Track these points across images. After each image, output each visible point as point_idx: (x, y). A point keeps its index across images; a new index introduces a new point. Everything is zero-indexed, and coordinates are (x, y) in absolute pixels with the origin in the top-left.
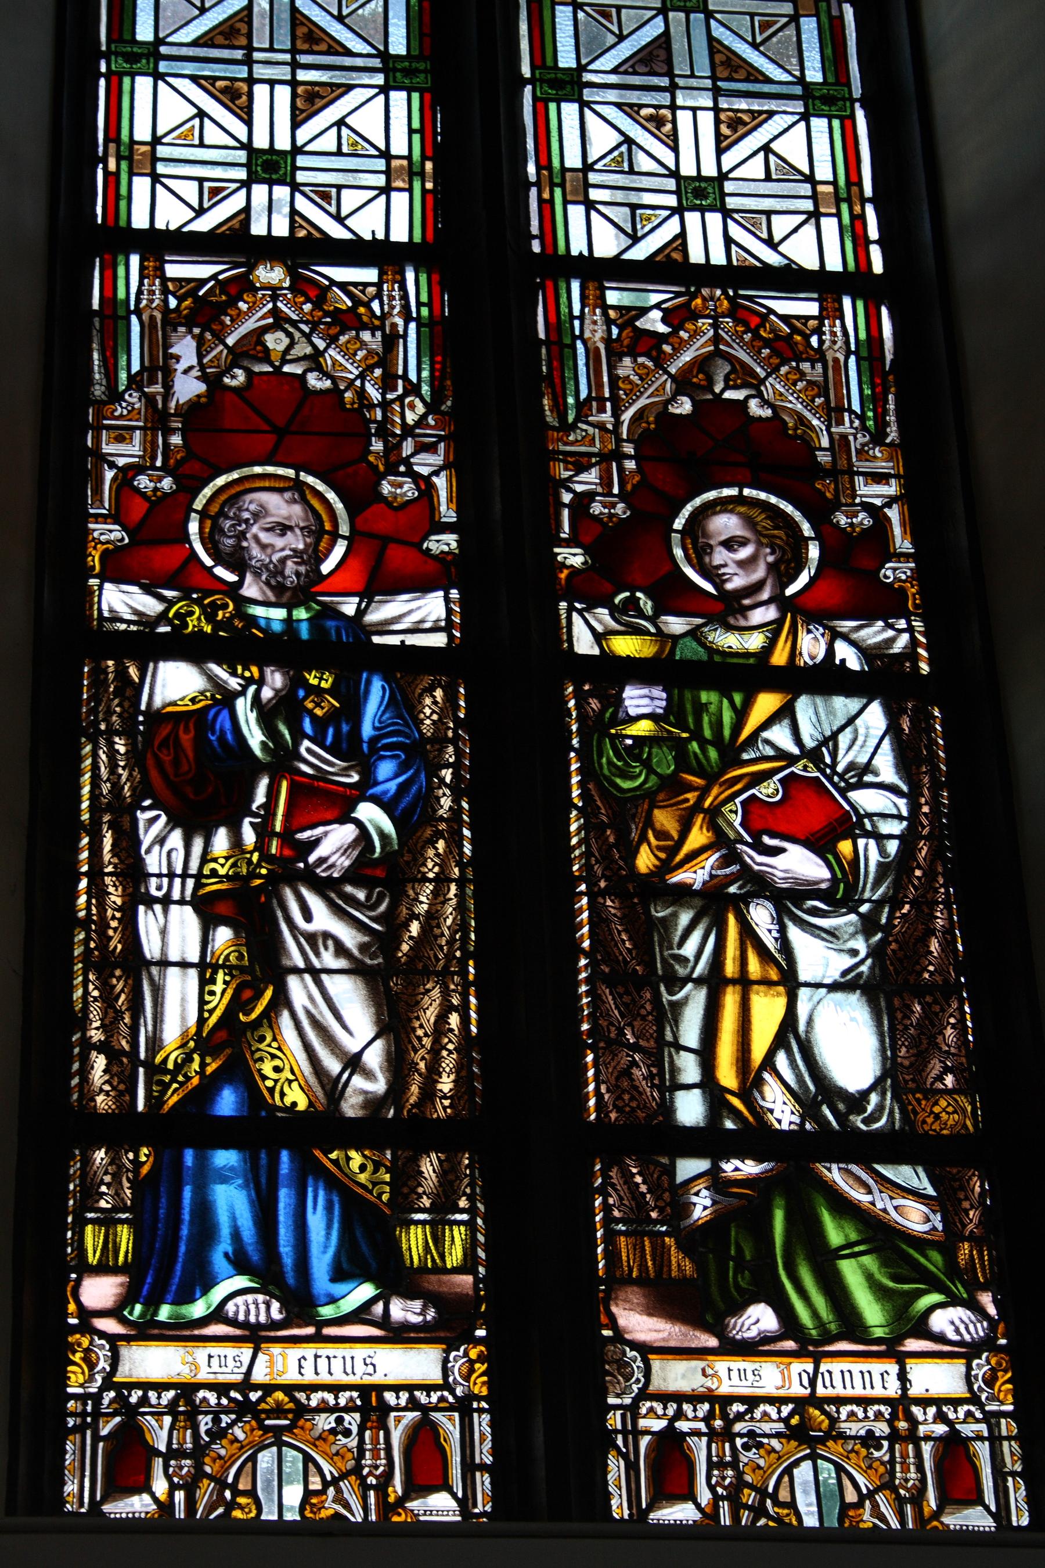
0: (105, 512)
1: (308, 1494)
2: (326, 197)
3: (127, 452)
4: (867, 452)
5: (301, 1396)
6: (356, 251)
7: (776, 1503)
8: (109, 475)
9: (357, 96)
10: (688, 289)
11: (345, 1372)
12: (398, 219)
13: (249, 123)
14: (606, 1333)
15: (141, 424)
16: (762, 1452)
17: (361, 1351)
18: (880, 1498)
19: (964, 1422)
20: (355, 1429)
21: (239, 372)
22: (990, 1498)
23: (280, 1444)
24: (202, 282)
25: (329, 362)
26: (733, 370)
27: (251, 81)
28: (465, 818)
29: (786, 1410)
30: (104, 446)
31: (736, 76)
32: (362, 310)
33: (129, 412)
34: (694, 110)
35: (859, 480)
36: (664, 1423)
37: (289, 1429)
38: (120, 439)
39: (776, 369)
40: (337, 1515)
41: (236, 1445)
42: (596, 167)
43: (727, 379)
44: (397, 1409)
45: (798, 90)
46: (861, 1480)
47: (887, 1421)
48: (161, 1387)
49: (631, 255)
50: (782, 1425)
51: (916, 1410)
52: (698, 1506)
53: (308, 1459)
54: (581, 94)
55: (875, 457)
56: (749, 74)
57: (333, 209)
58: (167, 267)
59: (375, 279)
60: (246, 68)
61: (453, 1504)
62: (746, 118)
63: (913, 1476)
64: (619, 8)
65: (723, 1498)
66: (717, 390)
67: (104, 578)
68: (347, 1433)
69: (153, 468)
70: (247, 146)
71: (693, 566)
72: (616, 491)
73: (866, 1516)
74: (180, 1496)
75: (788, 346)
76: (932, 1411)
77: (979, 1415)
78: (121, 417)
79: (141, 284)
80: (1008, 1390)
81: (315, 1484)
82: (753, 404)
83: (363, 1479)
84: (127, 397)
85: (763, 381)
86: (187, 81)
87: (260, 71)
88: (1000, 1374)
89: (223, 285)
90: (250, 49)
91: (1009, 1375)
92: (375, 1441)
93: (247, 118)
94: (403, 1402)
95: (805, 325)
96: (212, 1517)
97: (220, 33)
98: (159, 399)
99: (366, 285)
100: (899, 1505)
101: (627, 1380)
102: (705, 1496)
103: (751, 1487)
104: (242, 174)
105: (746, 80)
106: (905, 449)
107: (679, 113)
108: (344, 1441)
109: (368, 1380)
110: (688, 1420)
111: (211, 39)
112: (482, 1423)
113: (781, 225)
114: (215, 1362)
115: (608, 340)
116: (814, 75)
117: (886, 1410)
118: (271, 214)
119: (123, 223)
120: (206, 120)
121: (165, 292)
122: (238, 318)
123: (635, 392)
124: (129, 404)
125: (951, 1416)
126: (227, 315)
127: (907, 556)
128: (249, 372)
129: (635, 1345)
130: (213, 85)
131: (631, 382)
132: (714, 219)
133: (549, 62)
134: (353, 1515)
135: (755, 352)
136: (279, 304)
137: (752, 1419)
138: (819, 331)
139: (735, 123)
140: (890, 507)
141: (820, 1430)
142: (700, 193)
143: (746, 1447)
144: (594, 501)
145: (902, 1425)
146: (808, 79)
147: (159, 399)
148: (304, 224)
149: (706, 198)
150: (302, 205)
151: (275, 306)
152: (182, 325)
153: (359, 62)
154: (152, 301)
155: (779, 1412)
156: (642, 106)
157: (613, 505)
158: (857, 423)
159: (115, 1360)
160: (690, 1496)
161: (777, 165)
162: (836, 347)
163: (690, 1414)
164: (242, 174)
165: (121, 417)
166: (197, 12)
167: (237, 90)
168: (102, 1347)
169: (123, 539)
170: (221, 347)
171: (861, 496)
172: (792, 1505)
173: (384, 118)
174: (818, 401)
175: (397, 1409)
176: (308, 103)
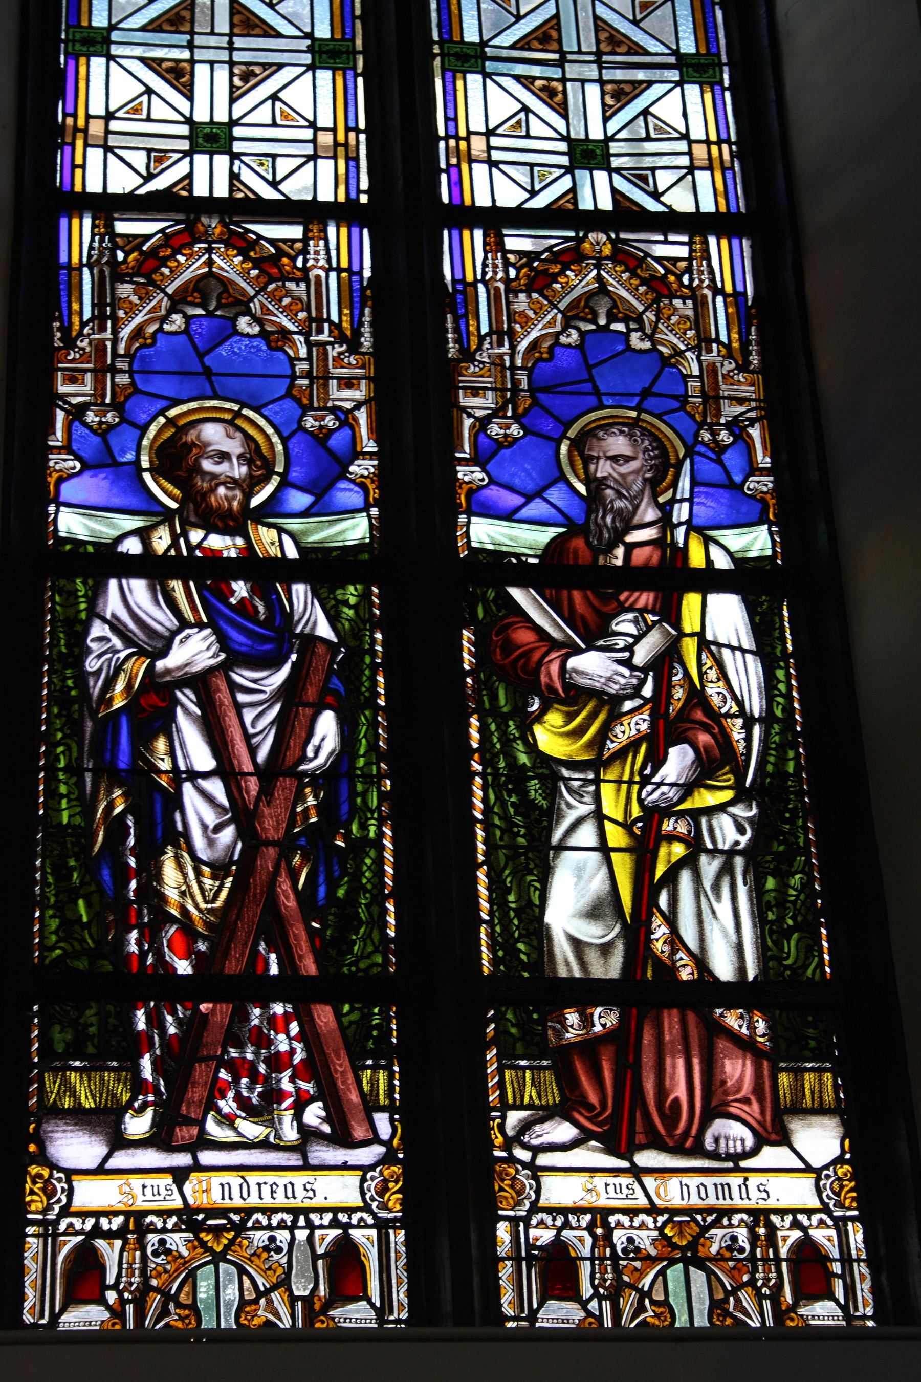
0: (59, 444)
1: (243, 1303)
4: (732, 377)
5: (699, 1218)
6: (670, 222)
7: (179, 1305)
8: (468, 422)
9: (657, 90)
10: (577, 234)
11: (287, 1197)
12: (703, 195)
13: (190, 98)
15: (91, 366)
16: (170, 1258)
18: (275, 1296)
19: (358, 1227)
22: (839, 1293)
25: (258, 306)
27: (564, 80)
28: (797, 717)
29: (661, 1219)
30: (60, 387)
31: (618, 50)
32: (672, 278)
33: (81, 355)
34: (583, 82)
35: (333, 383)
38: (73, 380)
39: (263, 289)
40: (268, 1322)
41: (181, 1261)
43: (219, 298)
44: (322, 1227)
45: (672, 60)
46: (260, 1281)
48: (111, 1214)
50: (656, 1233)
54: (483, 67)
55: (350, 364)
56: (630, 48)
58: (506, 239)
59: (300, 236)
61: (373, 1314)
63: (137, 1279)
65: (129, 1301)
66: (211, 308)
67: (470, 513)
68: (279, 1250)
69: (103, 404)
70: (189, 121)
71: (581, 481)
72: (108, 401)
76: (789, 1218)
77: (370, 1221)
78: (73, 361)
80: (853, 1198)
81: (249, 1295)
82: (635, 337)
83: (758, 1290)
84: (78, 343)
86: (137, 62)
88: (391, 1185)
89: (556, 257)
90: (192, 33)
91: (853, 1184)
93: (189, 94)
94: (326, 1222)
96: (157, 1327)
97: (535, 39)
98: (507, 358)
99: (294, 241)
101: (49, 1199)
104: (185, 145)
105: (627, 53)
108: (276, 1257)
109: (762, 1205)
111: (528, 43)
112: (398, 1237)
113: (664, 179)
114: (148, 1191)
115: (507, 280)
116: (688, 46)
119: (468, 202)
120: (154, 97)
121: (507, 264)
123: (527, 323)
124: (480, 362)
125: (806, 1223)
126: (557, 282)
127: (371, 454)
131: (527, 316)
133: (456, 38)
134: (282, 1321)
135: (633, 291)
136: (214, 256)
137: (731, 1226)
142: (212, 138)
143: (156, 1254)
144: (491, 423)
146: (682, 51)
148: (242, 188)
151: (599, 274)
152: (522, 291)
153: (657, 59)
154: (495, 273)
156: (535, 78)
157: (508, 427)
158: (724, 351)
159: (70, 1193)
162: (705, 285)
164: (185, 145)
166: (513, 20)
168: (59, 1180)
169: (483, 480)
170: (162, 295)
171: (334, 400)
173: (687, 110)
174: (690, 334)
175: (322, 1227)
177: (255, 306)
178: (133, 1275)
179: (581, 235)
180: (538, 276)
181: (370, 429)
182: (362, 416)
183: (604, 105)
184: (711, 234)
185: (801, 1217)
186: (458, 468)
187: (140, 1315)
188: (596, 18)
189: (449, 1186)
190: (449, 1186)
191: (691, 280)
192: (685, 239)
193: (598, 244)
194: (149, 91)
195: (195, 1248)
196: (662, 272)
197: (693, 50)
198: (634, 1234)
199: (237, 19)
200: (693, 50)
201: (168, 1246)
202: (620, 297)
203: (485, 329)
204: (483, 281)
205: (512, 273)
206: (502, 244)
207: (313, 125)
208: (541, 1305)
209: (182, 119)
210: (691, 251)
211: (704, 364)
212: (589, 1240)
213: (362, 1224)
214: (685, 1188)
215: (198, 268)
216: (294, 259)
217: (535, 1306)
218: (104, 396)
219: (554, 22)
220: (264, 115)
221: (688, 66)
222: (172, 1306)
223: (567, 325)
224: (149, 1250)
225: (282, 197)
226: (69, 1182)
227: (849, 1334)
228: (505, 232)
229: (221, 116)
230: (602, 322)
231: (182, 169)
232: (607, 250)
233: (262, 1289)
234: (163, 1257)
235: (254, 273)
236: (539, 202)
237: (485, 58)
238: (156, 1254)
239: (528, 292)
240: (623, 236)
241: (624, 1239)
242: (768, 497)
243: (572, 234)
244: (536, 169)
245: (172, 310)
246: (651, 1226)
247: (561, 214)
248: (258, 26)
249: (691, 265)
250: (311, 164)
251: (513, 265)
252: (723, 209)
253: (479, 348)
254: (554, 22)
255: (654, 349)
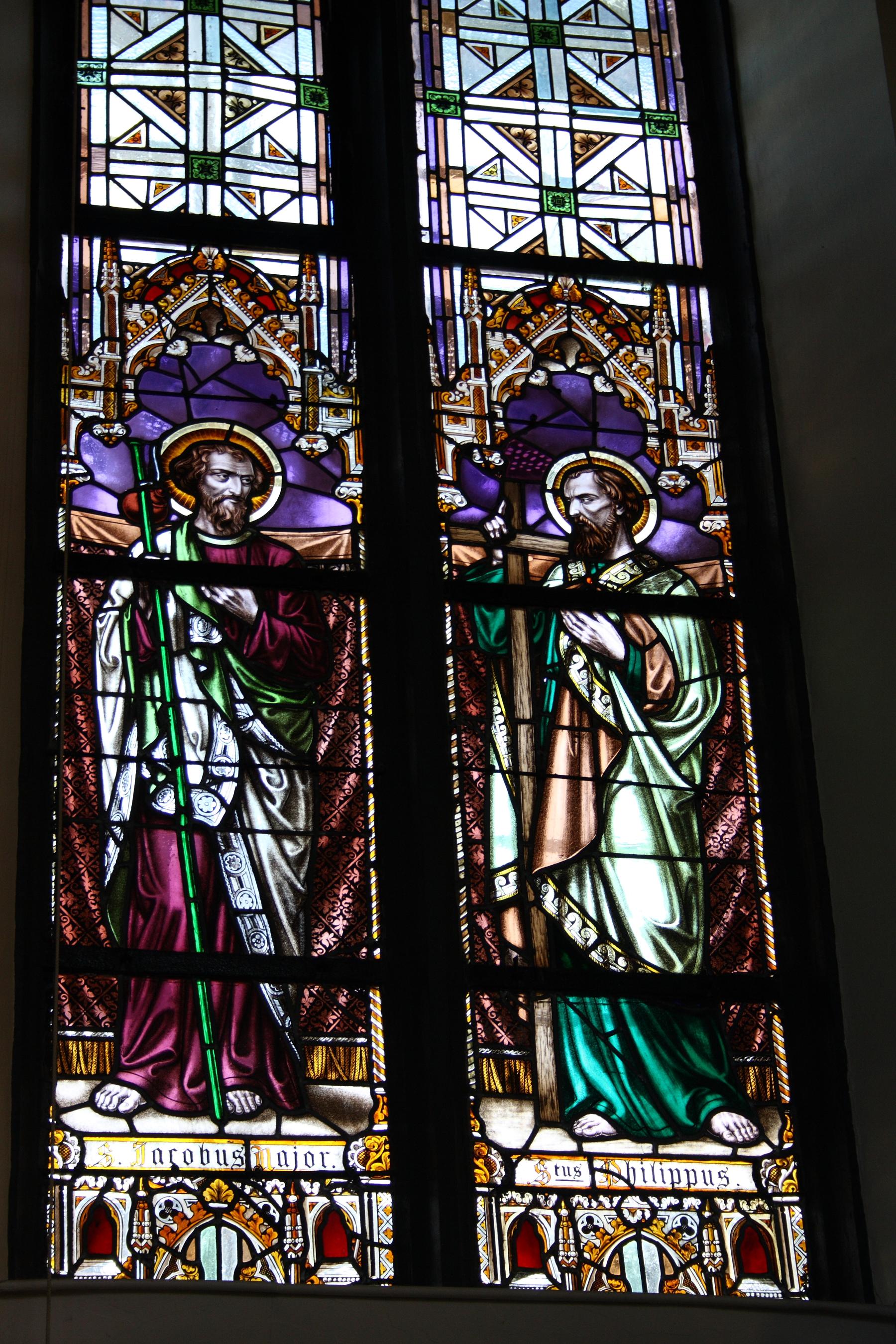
2: (604, 228)
3: (462, 433)
5: (654, 1200)
6: (632, 271)
7: (185, 1262)
8: (75, 423)
9: (621, 144)
10: (189, 248)
14: (476, 1134)
15: (100, 384)
17: (715, 1167)
19: (755, 1212)
20: (695, 1228)
21: (541, 373)
23: (219, 1224)
24: (151, 267)
26: (583, 349)
27: (537, 127)
29: (616, 1199)
34: (555, 129)
36: (523, 1209)
37: (227, 1211)
38: (84, 396)
39: (613, 353)
42: (118, 144)
43: (578, 357)
47: (697, 1211)
49: (503, 248)
51: (719, 1201)
52: (119, 1264)
53: (241, 1236)
57: (614, 241)
58: (123, 251)
60: (533, 117)
62: (596, 138)
64: (146, 10)
70: (184, 149)
73: (257, 1274)
74: (569, 1277)
75: (267, 299)
76: (731, 1201)
79: (101, 267)
81: (670, 1271)
83: (284, 1254)
85: (606, 360)
87: (544, 120)
89: (528, 297)
92: (294, 1223)
95: (286, 282)
97: (162, 51)
100: (286, 1263)
102: (125, 1254)
103: (590, 1262)
106: (361, 388)
107: (542, 131)
108: (688, 1237)
110: (116, 1191)
115: (121, 289)
117: (696, 1202)
118: (563, 240)
120: (151, 126)
121: (122, 274)
122: (540, 326)
123: (140, 334)
128: (190, 344)
129: (74, 1132)
130: (509, 131)
131: (138, 326)
132: (569, 224)
136: (573, 317)
138: (298, 288)
139: (587, 144)
140: (348, 435)
141: (226, 1202)
143: (163, 1214)
145: (293, 1199)
147: (485, 389)
149: (563, 206)
150: (586, 233)
152: (136, 302)
155: (611, 1202)
158: (680, 399)
160: (111, 1254)
161: (620, 180)
162: (113, 286)
163: (119, 1187)
165: (455, 402)
167: (177, 98)
172: (622, 1278)
176: (585, 148)
177: (251, 337)
178: (143, 1232)
179: (550, 279)
180: (151, 288)
181: (358, 456)
182: (350, 441)
183: (574, 153)
184: (671, 284)
185: (744, 1205)
186: (440, 489)
187: (150, 1271)
188: (568, 71)
189: (434, 1162)
190: (434, 1162)
191: (651, 330)
192: (296, 258)
193: (210, 257)
194: (147, 121)
195: (199, 1210)
196: (271, 288)
197: (654, 107)
198: (592, 1213)
199: (574, 88)
200: (654, 107)
201: (595, 1223)
202: (588, 342)
203: (97, 335)
204: (462, 315)
205: (127, 282)
206: (478, 282)
207: (648, 193)
208: (80, 1262)
209: (177, 148)
210: (653, 301)
211: (662, 412)
212: (554, 1219)
213: (760, 1210)
214: (205, 1153)
215: (199, 297)
216: (287, 293)
217: (508, 1275)
218: (484, 438)
219: (530, 71)
220: (604, 182)
221: (650, 120)
222: (179, 1262)
223: (536, 367)
224: (580, 1227)
225: (627, 260)
226: (81, 1144)
227: (786, 1306)
228: (123, 243)
229: (215, 146)
230: (571, 363)
231: (535, 229)
232: (220, 263)
233: (259, 1251)
234: (170, 1217)
235: (251, 305)
236: (510, 246)
237: (465, 106)
238: (586, 1230)
239: (505, 331)
240: (590, 282)
241: (584, 1218)
242: (357, 501)
243: (183, 248)
244: (510, 214)
245: (175, 337)
246: (608, 1205)
247: (529, 260)
248: (592, 96)
249: (652, 315)
250: (650, 228)
251: (128, 276)
252: (680, 260)
253: (91, 352)
254: (530, 71)
255: (258, 360)
